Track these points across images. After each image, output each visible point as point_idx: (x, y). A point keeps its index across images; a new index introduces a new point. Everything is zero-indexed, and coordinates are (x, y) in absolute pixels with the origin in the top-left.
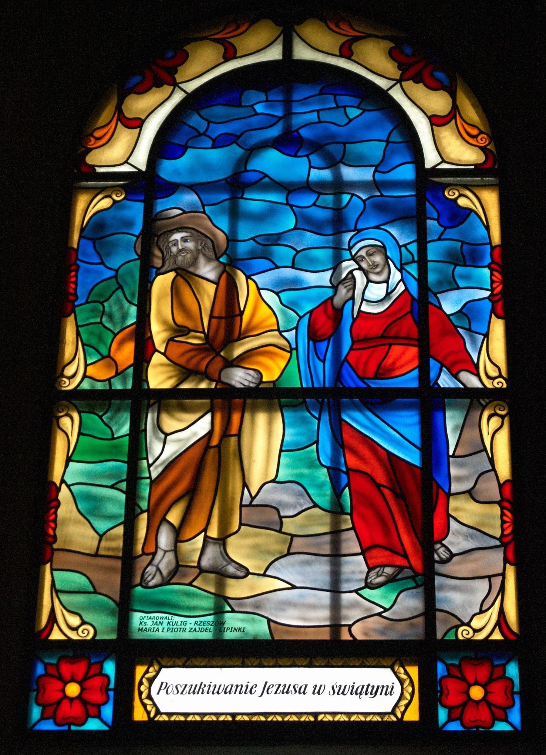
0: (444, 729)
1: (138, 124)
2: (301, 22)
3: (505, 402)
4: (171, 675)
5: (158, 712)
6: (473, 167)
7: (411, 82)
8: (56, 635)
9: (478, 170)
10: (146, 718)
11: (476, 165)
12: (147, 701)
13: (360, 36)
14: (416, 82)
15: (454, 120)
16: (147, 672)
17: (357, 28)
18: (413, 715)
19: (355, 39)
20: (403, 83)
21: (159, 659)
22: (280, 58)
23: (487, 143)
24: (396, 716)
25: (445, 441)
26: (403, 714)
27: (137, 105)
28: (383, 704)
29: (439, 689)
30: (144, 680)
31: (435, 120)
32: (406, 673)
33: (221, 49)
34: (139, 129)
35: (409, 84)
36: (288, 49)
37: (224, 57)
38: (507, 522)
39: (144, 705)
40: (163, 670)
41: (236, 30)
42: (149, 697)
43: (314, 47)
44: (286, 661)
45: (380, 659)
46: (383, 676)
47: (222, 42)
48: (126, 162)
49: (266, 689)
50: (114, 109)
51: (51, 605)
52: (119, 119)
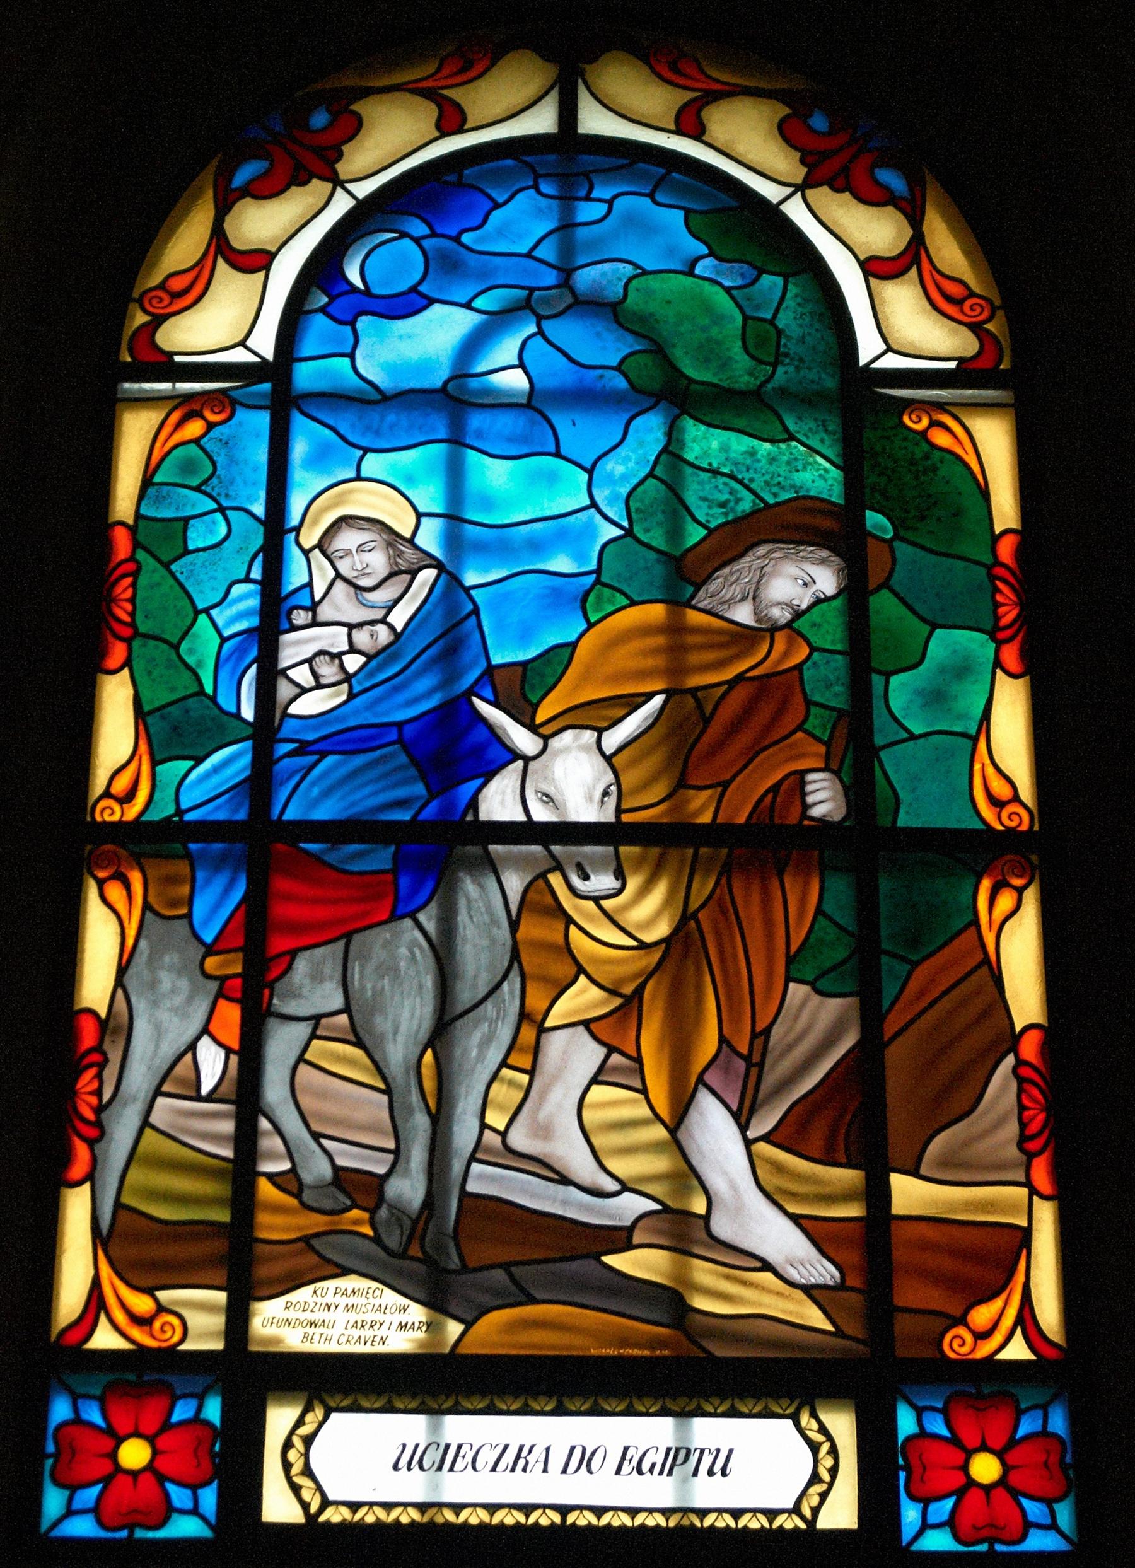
0: (915, 1547)
1: (257, 261)
2: (593, 59)
5: (326, 1503)
6: (952, 365)
7: (825, 189)
8: (104, 1339)
9: (965, 374)
11: (961, 360)
14: (837, 190)
17: (714, 74)
18: (841, 1512)
24: (802, 1517)
25: (230, 926)
26: (816, 1511)
27: (256, 223)
29: (901, 1462)
31: (874, 267)
32: (823, 1430)
35: (821, 195)
36: (568, 114)
37: (438, 126)
38: (91, 1093)
40: (334, 1415)
45: (770, 1400)
48: (242, 343)
51: (92, 1272)
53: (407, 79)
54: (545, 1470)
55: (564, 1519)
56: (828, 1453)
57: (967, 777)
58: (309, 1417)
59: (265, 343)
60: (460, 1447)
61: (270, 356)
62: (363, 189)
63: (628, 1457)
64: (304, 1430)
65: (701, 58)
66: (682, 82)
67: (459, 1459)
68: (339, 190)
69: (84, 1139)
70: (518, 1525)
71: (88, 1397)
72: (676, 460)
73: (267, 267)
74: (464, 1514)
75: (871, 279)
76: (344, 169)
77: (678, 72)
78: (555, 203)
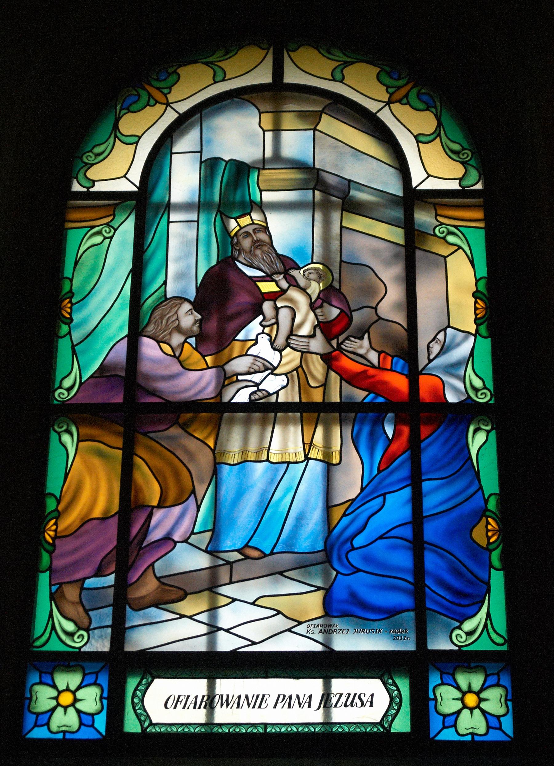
5: (151, 724)
7: (398, 104)
10: (138, 730)
13: (350, 62)
18: (402, 724)
19: (346, 64)
22: (271, 82)
23: (469, 158)
28: (373, 714)
40: (157, 681)
41: (225, 55)
46: (373, 686)
52: (116, 137)
54: (309, 707)
57: (103, 315)
60: (264, 696)
62: (183, 108)
63: (180, 700)
66: (330, 56)
67: (264, 702)
68: (169, 108)
71: (46, 673)
73: (137, 143)
77: (329, 52)
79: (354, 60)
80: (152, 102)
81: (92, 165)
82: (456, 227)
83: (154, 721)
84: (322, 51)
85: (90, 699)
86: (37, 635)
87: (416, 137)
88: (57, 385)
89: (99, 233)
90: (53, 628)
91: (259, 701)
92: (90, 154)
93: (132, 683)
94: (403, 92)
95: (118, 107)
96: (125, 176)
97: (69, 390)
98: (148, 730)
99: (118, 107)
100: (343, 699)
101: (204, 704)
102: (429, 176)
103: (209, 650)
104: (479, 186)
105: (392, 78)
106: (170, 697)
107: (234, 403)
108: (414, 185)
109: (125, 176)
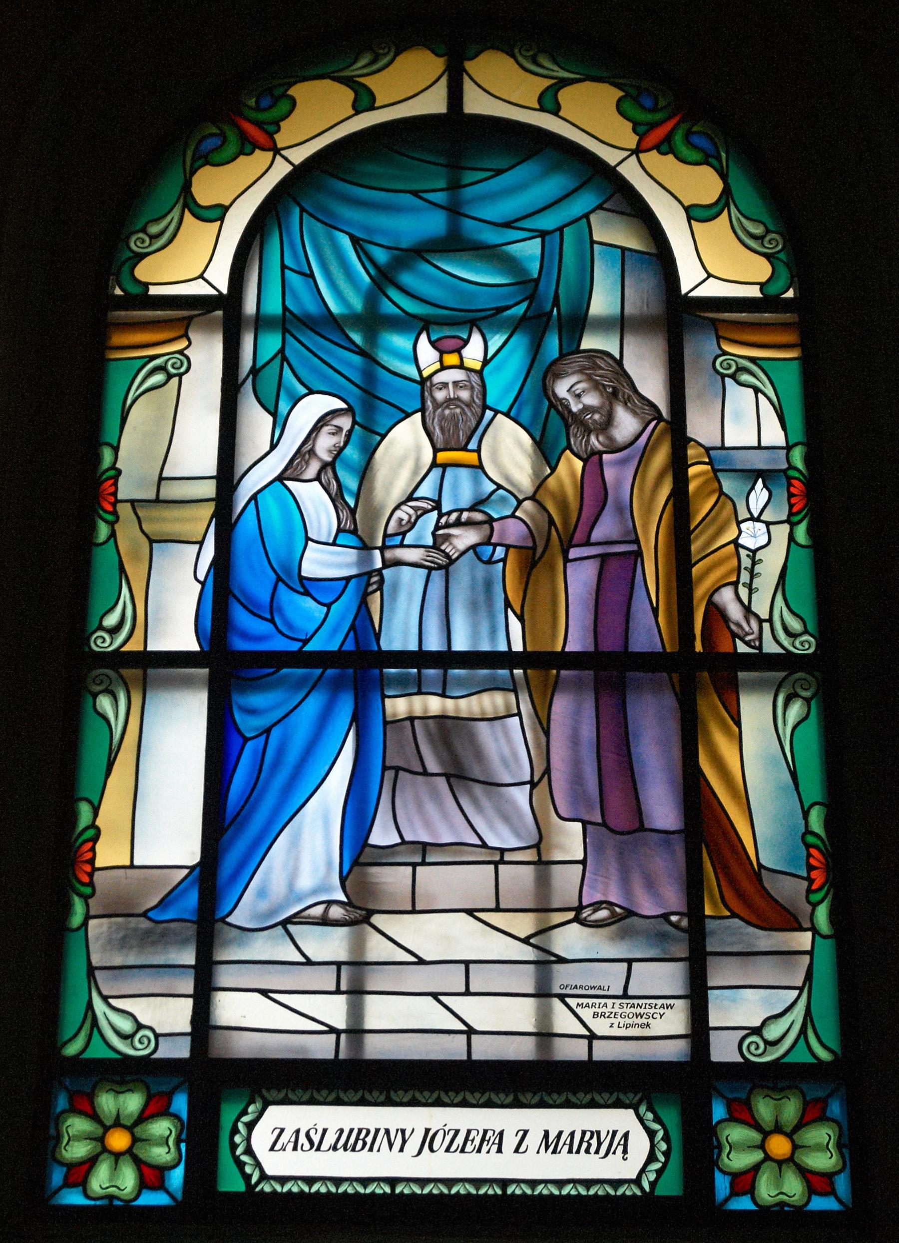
1: (218, 214)
3: (813, 676)
4: (278, 1116)
5: (264, 1177)
12: (244, 1158)
13: (572, 79)
15: (726, 210)
16: (244, 1112)
18: (671, 1186)
19: (563, 83)
20: (641, 155)
21: (264, 1092)
28: (624, 1167)
30: (240, 1126)
33: (350, 95)
34: (219, 222)
35: (651, 158)
36: (455, 96)
37: (354, 107)
39: (241, 1165)
42: (249, 1151)
43: (501, 89)
44: (351, 1095)
46: (622, 1120)
47: (349, 82)
49: (428, 1140)
50: (179, 190)
52: (186, 205)
53: (333, 69)
54: (499, 1151)
55: (393, 1189)
56: (662, 1139)
58: (251, 1109)
59: (220, 278)
60: (469, 1132)
61: (225, 291)
62: (299, 156)
64: (246, 1119)
65: (569, 44)
67: (469, 1143)
69: (80, 895)
70: (442, 1194)
72: (366, 425)
73: (222, 219)
74: (539, 1189)
75: (692, 222)
76: (281, 140)
78: (444, 170)
79: (578, 76)
80: (247, 146)
81: (143, 256)
82: (753, 360)
83: (269, 1172)
84: (520, 59)
85: (163, 1139)
86: (68, 1034)
87: (687, 209)
88: (95, 625)
89: (162, 368)
90: (95, 1023)
91: (459, 1142)
92: (141, 235)
93: (228, 1114)
94: (661, 132)
95: (189, 153)
96: (201, 276)
97: (114, 631)
98: (258, 1189)
99: (189, 153)
100: (460, 1140)
101: (585, 1145)
102: (710, 275)
103: (540, 1058)
104: (790, 294)
105: (642, 107)
106: (438, 1131)
107: (307, 652)
108: (684, 291)
109: (201, 276)
